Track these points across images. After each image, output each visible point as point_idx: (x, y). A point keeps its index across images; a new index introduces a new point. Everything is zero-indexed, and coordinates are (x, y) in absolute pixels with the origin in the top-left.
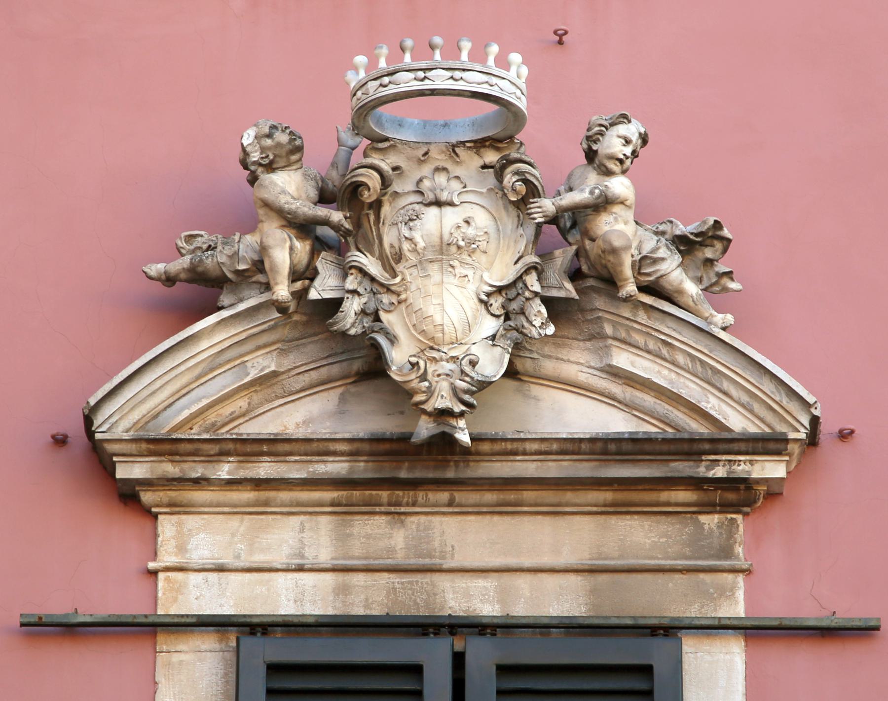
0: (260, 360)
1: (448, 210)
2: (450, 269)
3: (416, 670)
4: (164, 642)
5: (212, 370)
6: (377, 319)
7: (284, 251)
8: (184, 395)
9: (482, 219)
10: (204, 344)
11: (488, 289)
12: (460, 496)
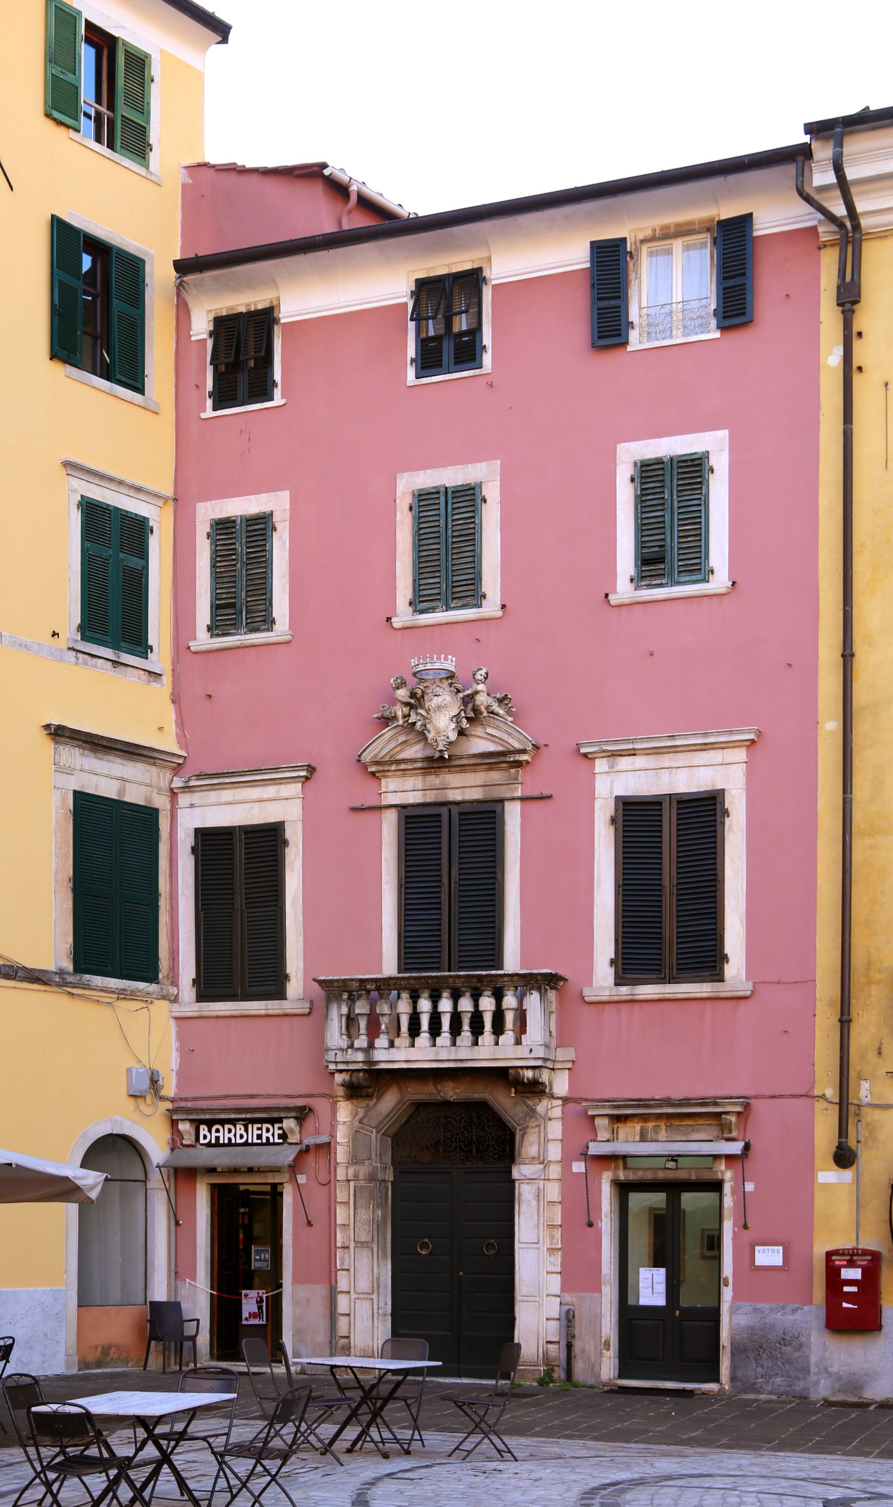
3: (439, 815)
4: (383, 811)
7: (400, 711)
9: (448, 698)
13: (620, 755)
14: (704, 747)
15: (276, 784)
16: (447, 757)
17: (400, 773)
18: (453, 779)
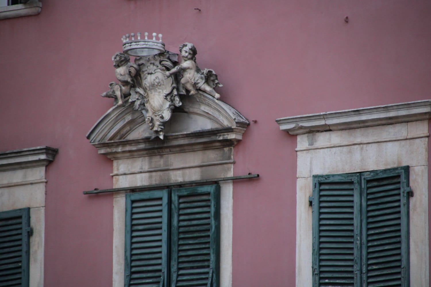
0: (128, 117)
1: (152, 75)
2: (156, 91)
5: (116, 123)
6: (144, 106)
8: (112, 129)
10: (112, 116)
11: (165, 95)
12: (172, 150)
13: (318, 131)
14: (390, 121)
15: (23, 168)
16: (161, 137)
17: (128, 154)
18: (176, 160)
